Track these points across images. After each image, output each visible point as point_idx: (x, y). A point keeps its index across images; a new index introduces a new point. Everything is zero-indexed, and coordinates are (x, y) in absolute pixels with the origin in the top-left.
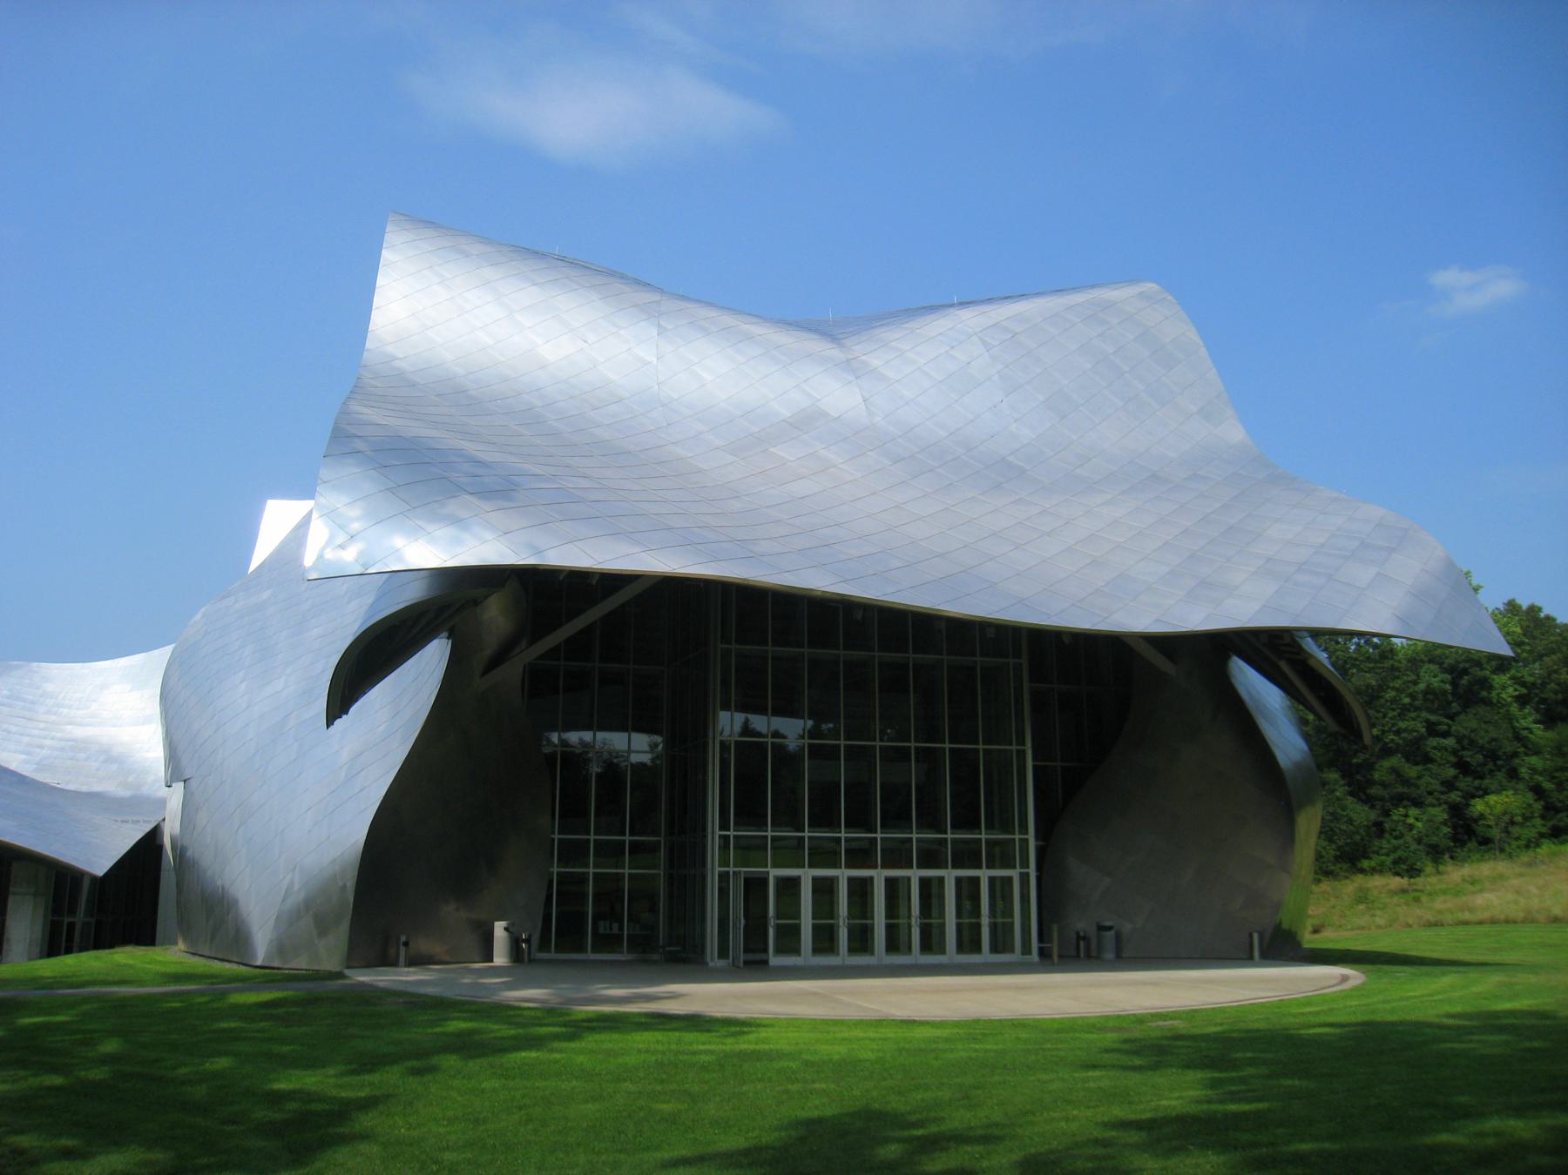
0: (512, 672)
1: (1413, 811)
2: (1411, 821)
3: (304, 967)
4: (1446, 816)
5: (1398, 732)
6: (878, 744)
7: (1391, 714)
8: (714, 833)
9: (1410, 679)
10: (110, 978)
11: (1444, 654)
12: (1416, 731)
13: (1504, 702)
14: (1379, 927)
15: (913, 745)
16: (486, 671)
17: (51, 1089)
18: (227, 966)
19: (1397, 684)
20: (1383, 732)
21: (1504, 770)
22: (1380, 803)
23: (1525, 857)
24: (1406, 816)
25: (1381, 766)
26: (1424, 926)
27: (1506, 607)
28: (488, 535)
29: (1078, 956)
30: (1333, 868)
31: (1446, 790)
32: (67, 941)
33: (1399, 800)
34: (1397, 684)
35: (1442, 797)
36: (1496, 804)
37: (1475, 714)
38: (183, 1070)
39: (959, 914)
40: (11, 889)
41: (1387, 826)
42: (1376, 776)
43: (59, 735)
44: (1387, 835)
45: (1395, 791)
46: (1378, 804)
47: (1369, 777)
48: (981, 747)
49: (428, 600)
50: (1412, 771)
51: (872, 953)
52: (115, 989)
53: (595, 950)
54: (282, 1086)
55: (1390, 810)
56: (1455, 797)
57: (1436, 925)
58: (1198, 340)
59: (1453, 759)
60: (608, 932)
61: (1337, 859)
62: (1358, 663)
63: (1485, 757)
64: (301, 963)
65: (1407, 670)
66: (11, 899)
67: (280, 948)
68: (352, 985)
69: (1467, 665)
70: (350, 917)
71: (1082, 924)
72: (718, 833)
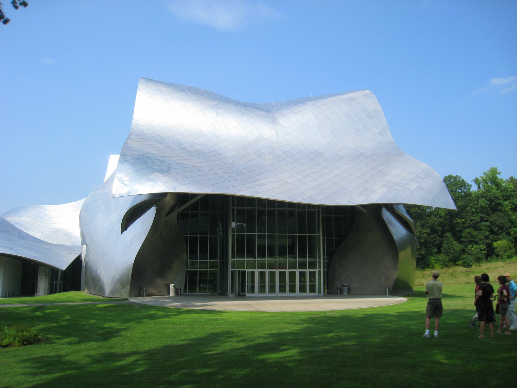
0: (174, 215)
1: (475, 246)
3: (118, 297)
4: (485, 247)
5: (471, 220)
6: (277, 234)
7: (469, 214)
8: (230, 260)
9: (475, 203)
10: (67, 300)
11: (487, 195)
12: (476, 220)
13: (506, 210)
14: (452, 284)
16: (166, 216)
17: (53, 326)
18: (98, 297)
19: (471, 205)
20: (466, 220)
21: (505, 233)
22: (465, 243)
23: (508, 261)
25: (465, 231)
26: (465, 283)
27: (510, 179)
28: (161, 184)
29: (337, 294)
30: (448, 264)
31: (486, 239)
32: (55, 289)
33: (470, 242)
34: (471, 205)
35: (484, 241)
36: (500, 244)
37: (496, 215)
38: (84, 323)
40: (39, 274)
41: (466, 251)
42: (464, 234)
43: (51, 227)
44: (466, 253)
45: (469, 239)
46: (464, 243)
47: (461, 235)
48: (307, 235)
49: (149, 199)
50: (475, 233)
51: (296, 293)
52: (68, 303)
53: (199, 292)
54: (105, 326)
55: (467, 246)
56: (488, 241)
57: (468, 283)
58: (381, 110)
59: (488, 229)
60: (203, 287)
61: (450, 261)
62: (458, 198)
63: (499, 228)
64: (118, 296)
65: (475, 200)
66: (39, 277)
67: (112, 292)
68: (130, 302)
69: (494, 199)
70: (130, 284)
71: (339, 285)
72: (231, 259)
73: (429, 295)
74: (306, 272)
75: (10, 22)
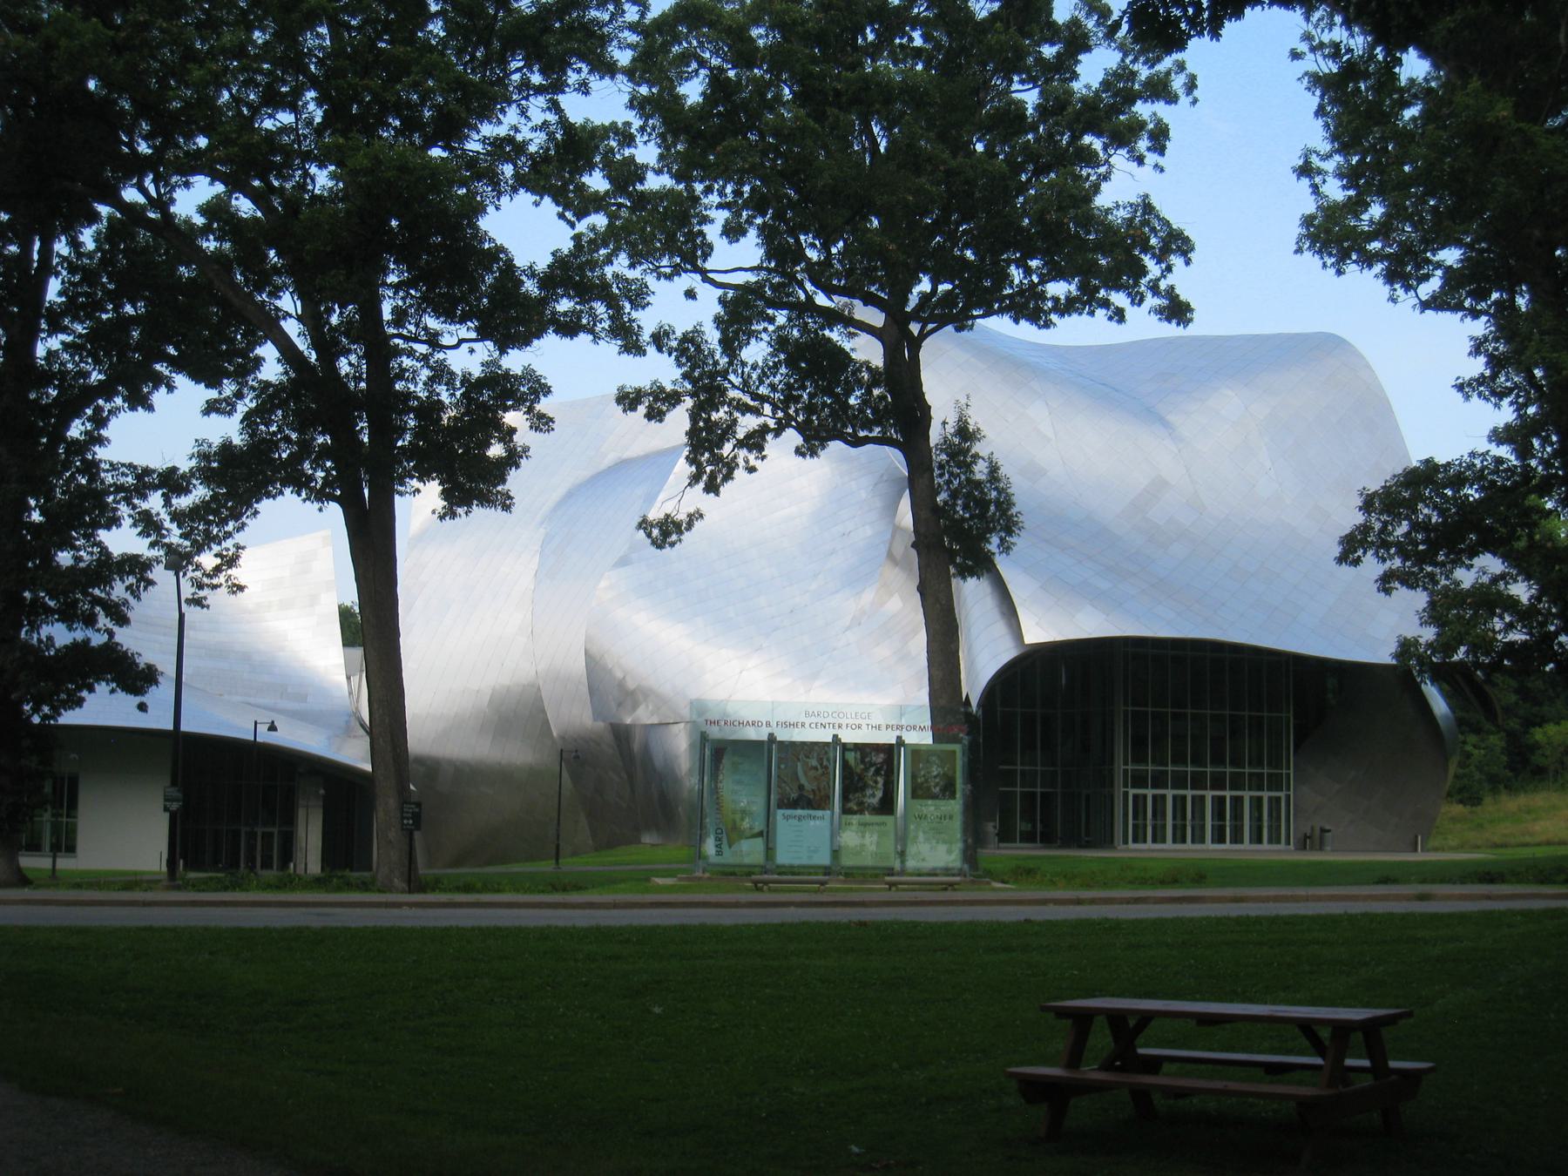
2: (1469, 748)
15: (1246, 713)
24: (1464, 742)
39: (1174, 818)
73: (975, 873)
74: (1242, 797)
75: (1014, 324)
